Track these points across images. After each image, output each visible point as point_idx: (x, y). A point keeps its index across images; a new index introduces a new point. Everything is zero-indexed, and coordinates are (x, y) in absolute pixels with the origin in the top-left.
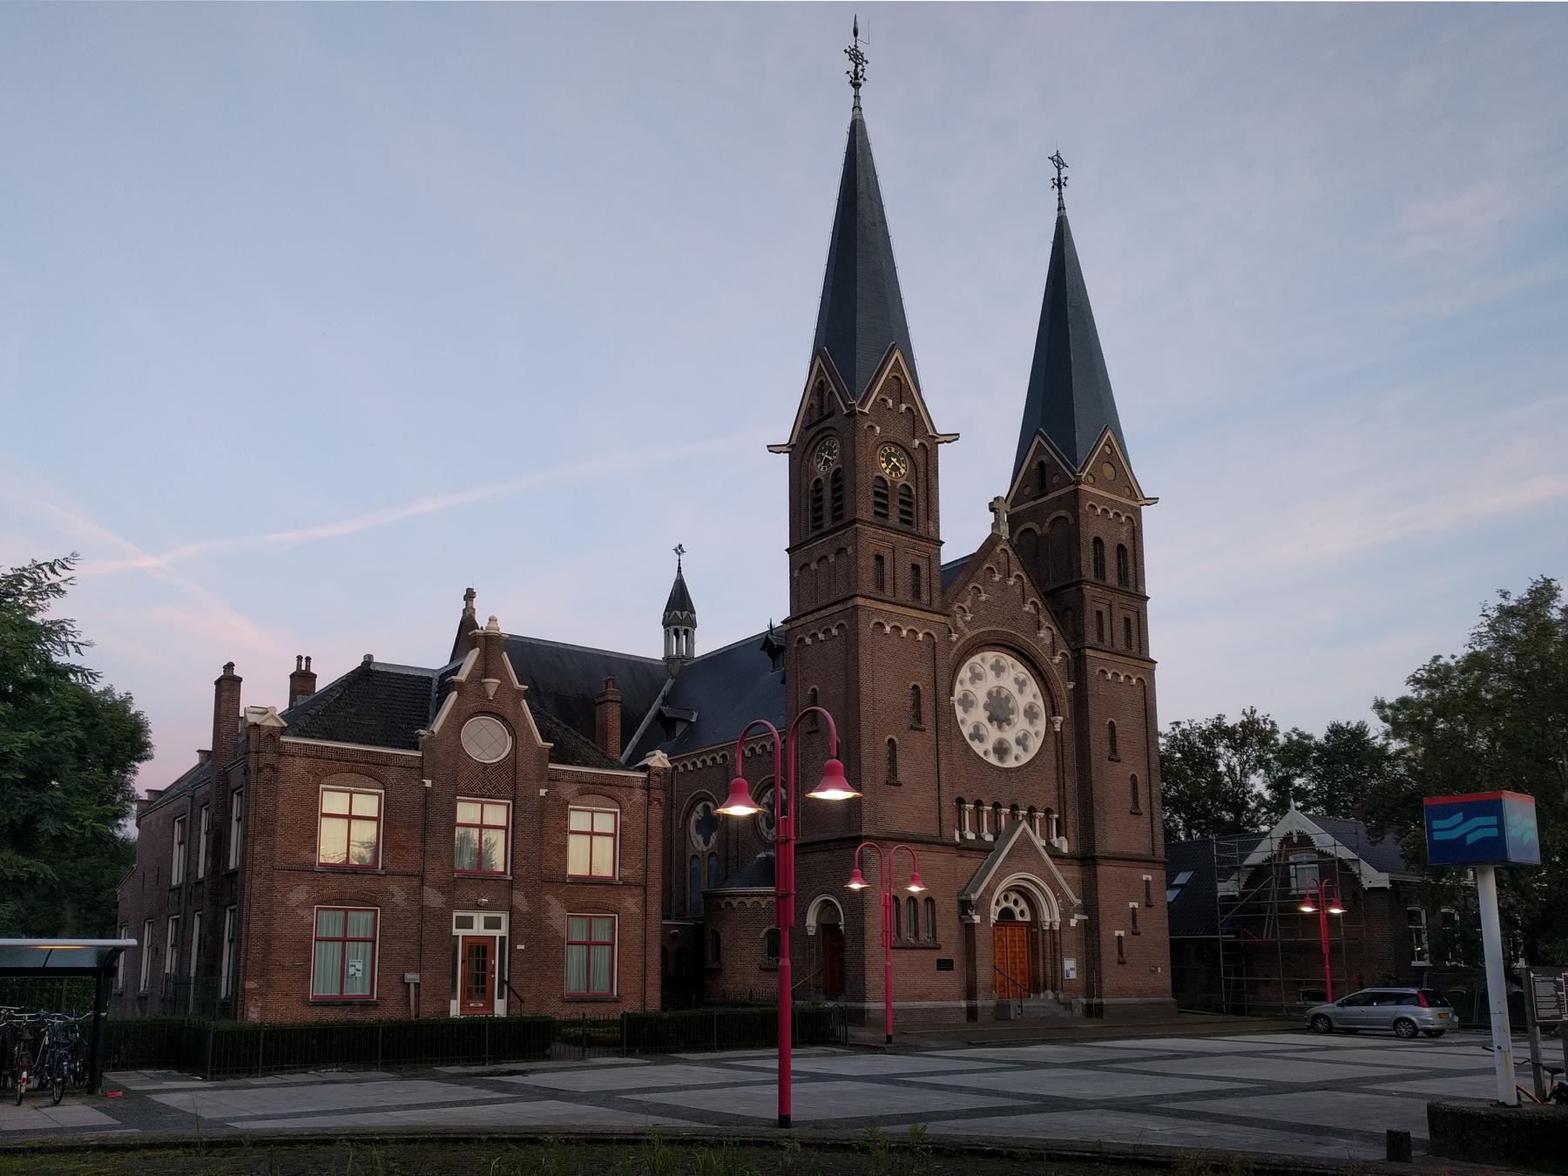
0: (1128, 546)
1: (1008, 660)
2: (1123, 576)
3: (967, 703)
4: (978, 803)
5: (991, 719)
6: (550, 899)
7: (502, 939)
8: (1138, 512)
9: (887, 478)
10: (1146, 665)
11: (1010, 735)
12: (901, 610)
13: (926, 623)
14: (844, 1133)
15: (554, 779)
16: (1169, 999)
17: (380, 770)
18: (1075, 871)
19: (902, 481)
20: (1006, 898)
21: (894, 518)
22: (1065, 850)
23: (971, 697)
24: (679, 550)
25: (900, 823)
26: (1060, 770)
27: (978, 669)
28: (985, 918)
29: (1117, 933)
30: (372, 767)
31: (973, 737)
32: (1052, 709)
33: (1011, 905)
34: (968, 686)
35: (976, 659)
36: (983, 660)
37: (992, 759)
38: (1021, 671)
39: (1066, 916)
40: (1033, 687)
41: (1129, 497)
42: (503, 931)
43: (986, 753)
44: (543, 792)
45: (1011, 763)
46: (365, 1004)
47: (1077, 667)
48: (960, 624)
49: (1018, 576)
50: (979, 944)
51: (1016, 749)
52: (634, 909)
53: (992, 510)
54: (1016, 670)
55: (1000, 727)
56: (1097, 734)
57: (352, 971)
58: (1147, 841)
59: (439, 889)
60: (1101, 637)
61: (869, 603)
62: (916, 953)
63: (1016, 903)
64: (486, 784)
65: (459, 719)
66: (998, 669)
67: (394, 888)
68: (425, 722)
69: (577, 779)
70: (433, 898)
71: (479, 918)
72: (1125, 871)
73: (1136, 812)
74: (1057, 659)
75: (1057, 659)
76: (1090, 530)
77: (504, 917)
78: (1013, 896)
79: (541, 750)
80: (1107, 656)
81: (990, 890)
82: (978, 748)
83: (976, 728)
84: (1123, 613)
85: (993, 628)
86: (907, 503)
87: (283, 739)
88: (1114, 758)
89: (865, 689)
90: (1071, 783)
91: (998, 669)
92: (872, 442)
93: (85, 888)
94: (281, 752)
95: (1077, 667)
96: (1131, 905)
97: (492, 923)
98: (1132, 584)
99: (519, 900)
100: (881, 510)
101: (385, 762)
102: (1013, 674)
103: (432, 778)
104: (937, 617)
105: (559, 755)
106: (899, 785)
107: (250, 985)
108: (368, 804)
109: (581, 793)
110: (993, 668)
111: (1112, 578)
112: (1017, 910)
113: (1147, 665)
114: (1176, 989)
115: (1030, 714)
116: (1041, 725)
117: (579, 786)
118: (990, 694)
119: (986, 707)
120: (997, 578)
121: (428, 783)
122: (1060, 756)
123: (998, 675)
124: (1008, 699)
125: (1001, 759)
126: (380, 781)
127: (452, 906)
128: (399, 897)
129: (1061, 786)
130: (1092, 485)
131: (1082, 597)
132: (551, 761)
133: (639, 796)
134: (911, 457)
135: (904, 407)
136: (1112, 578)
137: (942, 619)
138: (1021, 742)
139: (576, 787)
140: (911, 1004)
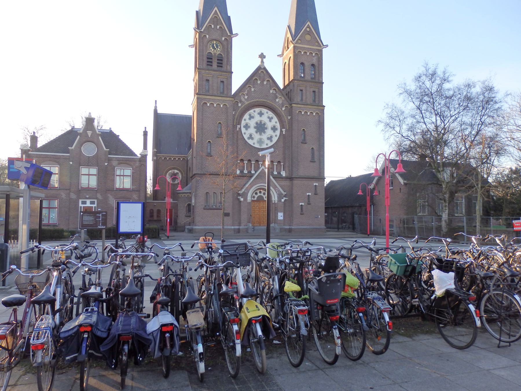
0: (316, 64)
1: (264, 110)
3: (247, 127)
4: (249, 161)
6: (109, 195)
8: (321, 51)
9: (212, 53)
10: (320, 108)
11: (264, 137)
12: (219, 98)
13: (224, 101)
19: (219, 53)
23: (249, 125)
25: (212, 169)
27: (252, 115)
28: (246, 199)
34: (248, 121)
35: (251, 111)
36: (254, 111)
38: (271, 114)
39: (280, 196)
40: (275, 119)
41: (317, 46)
42: (95, 205)
43: (254, 144)
44: (106, 164)
46: (54, 225)
47: (290, 111)
48: (243, 100)
49: (268, 80)
50: (242, 207)
54: (267, 113)
57: (51, 216)
62: (215, 211)
64: (89, 162)
65: (81, 144)
66: (261, 114)
67: (62, 193)
70: (73, 196)
71: (88, 201)
72: (305, 182)
73: (313, 161)
75: (284, 109)
77: (96, 201)
78: (258, 192)
79: (106, 151)
80: (302, 106)
81: (248, 189)
83: (251, 135)
84: (312, 90)
85: (258, 100)
87: (30, 153)
88: (304, 142)
91: (261, 114)
95: (290, 111)
97: (92, 203)
99: (99, 196)
101: (58, 158)
103: (72, 161)
109: (119, 164)
110: (258, 114)
113: (322, 108)
114: (327, 222)
115: (274, 129)
116: (278, 133)
118: (257, 123)
119: (261, 134)
120: (259, 82)
121: (71, 163)
123: (261, 116)
126: (130, 165)
127: (79, 198)
130: (300, 44)
132: (110, 155)
134: (222, 44)
135: (218, 27)
138: (270, 119)
139: (117, 162)
140: (212, 227)
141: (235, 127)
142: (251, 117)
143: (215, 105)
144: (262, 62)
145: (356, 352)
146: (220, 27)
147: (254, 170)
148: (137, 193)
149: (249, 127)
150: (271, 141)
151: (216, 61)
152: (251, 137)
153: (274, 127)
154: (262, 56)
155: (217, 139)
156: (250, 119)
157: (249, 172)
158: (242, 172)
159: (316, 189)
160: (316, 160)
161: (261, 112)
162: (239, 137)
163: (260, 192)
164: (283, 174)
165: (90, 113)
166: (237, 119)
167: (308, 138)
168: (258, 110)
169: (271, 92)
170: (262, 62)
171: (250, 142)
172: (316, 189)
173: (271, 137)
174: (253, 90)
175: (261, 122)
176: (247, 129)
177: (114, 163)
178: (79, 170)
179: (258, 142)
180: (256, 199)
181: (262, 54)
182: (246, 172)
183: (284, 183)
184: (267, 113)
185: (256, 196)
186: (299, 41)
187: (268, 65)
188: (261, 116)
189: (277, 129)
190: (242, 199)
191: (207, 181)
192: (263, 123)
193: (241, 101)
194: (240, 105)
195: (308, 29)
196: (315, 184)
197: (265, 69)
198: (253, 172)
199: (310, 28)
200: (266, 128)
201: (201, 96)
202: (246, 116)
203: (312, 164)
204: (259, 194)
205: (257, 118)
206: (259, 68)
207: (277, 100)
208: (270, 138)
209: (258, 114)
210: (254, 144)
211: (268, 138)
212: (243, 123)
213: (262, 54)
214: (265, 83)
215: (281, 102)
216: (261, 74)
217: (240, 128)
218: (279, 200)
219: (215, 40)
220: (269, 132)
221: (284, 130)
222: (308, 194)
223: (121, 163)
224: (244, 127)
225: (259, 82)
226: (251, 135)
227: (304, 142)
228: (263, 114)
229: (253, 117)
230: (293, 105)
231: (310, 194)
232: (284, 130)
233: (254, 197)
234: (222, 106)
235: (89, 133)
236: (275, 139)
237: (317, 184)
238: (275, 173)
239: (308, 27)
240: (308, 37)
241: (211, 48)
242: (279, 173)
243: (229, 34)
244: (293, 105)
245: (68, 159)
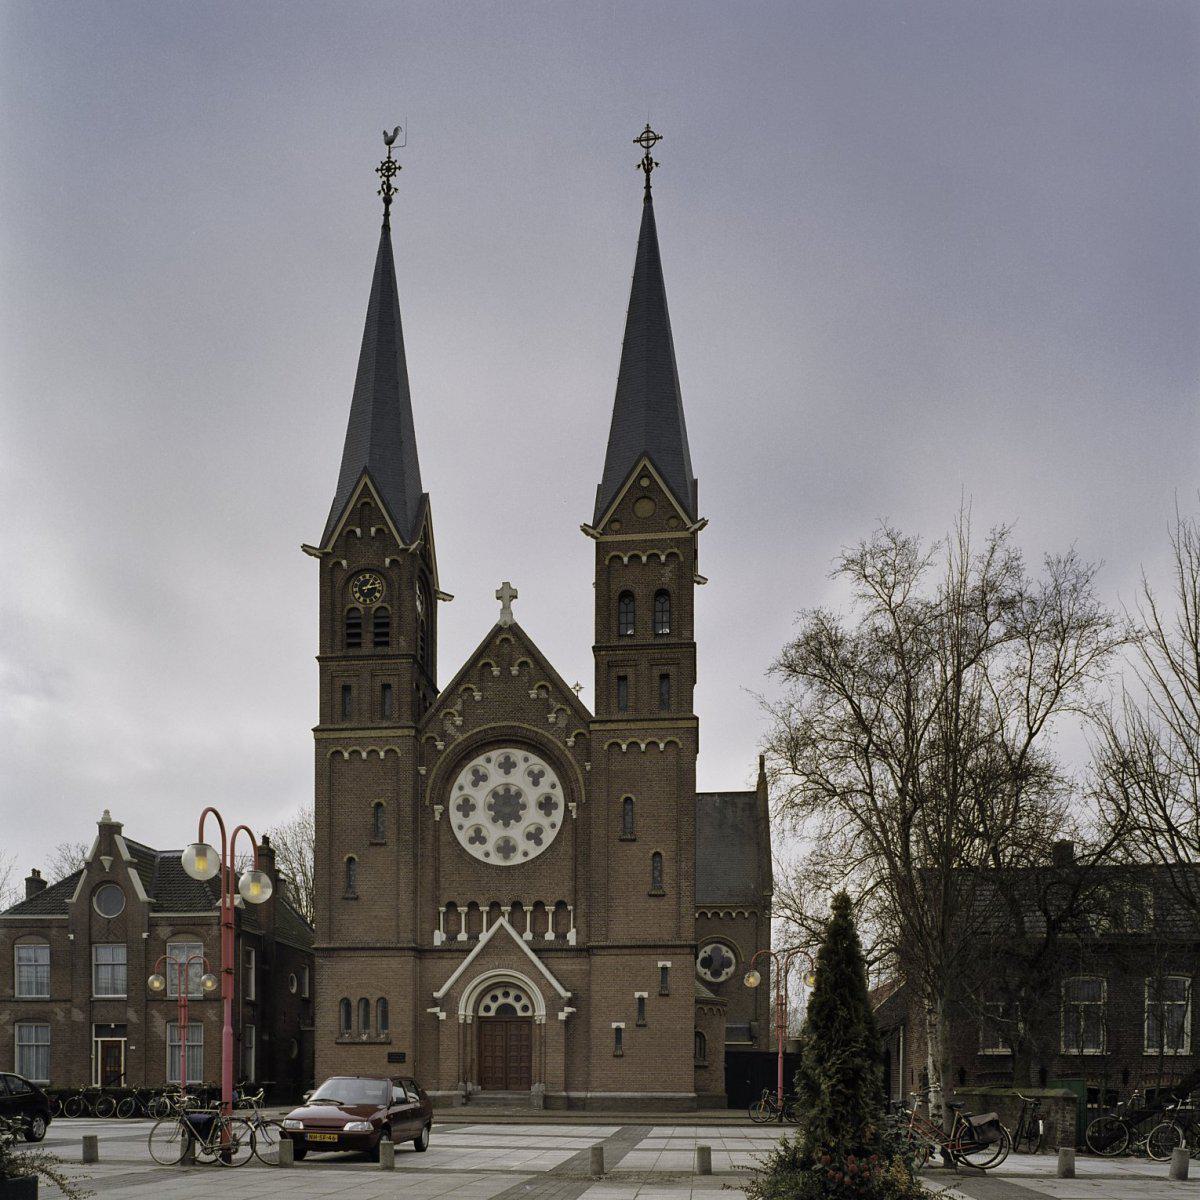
1: (517, 755)
3: (467, 807)
5: (518, 819)
8: (692, 542)
9: (361, 607)
13: (387, 740)
14: (206, 1169)
16: (725, 1094)
17: (202, 930)
19: (378, 604)
21: (368, 638)
23: (472, 801)
27: (482, 771)
28: (452, 1012)
30: (42, 930)
31: (472, 841)
32: (569, 796)
33: (510, 1000)
35: (479, 761)
37: (496, 860)
40: (551, 776)
44: (145, 935)
45: (517, 859)
48: (451, 730)
52: (214, 1018)
53: (498, 598)
54: (489, 762)
59: (80, 1009)
67: (57, 1010)
69: (171, 922)
75: (571, 742)
83: (478, 831)
85: (493, 725)
86: (353, 637)
91: (507, 766)
93: (1186, 1121)
101: (48, 925)
108: (44, 956)
109: (174, 934)
110: (500, 766)
115: (546, 805)
116: (558, 816)
117: (171, 928)
120: (496, 671)
123: (507, 772)
124: (519, 794)
125: (506, 857)
128: (60, 1016)
130: (617, 532)
138: (536, 777)
143: (364, 755)
144: (506, 609)
146: (378, 531)
147: (468, 931)
148: (149, 998)
149: (473, 807)
150: (539, 842)
151: (372, 629)
152: (478, 837)
153: (548, 798)
154: (507, 594)
155: (373, 849)
156: (475, 784)
159: (664, 980)
160: (667, 889)
161: (507, 758)
162: (444, 838)
165: (107, 812)
166: (432, 789)
168: (496, 755)
169: (533, 694)
170: (506, 609)
171: (476, 851)
172: (664, 980)
173: (539, 830)
174: (477, 696)
175: (507, 790)
176: (548, 798)
179: (499, 849)
180: (492, 1013)
181: (506, 585)
183: (568, 965)
184: (526, 760)
185: (494, 1006)
187: (525, 617)
188: (507, 772)
189: (555, 806)
190: (443, 1016)
191: (345, 966)
192: (513, 790)
193: (444, 736)
196: (660, 964)
197: (515, 629)
199: (650, 476)
201: (325, 735)
202: (465, 777)
203: (652, 902)
204: (501, 1000)
205: (517, 832)
206: (498, 630)
207: (552, 718)
208: (535, 836)
209: (514, 849)
210: (487, 855)
211: (529, 836)
212: (455, 797)
213: (506, 585)
214: (515, 671)
215: (562, 723)
216: (508, 647)
217: (445, 814)
220: (532, 816)
222: (637, 995)
224: (459, 808)
225: (496, 671)
226: (478, 831)
228: (514, 765)
229: (484, 778)
231: (645, 995)
233: (487, 1009)
234: (382, 754)
235: (106, 860)
236: (549, 837)
237: (669, 964)
239: (645, 474)
241: (357, 595)
245: (64, 927)
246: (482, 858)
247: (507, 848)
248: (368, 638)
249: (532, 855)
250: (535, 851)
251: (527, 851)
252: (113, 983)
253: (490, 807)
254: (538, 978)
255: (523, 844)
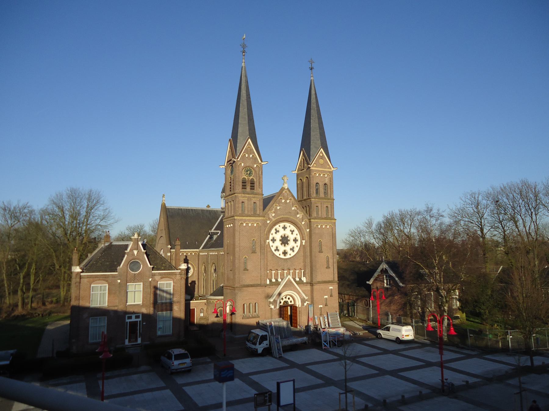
1: (287, 224)
2: (326, 193)
3: (274, 240)
7: (140, 321)
10: (333, 221)
11: (288, 248)
13: (257, 221)
15: (153, 275)
18: (308, 288)
20: (286, 297)
21: (248, 188)
22: (305, 281)
24: (311, 69)
25: (248, 282)
26: (305, 257)
29: (320, 306)
31: (275, 250)
32: (302, 238)
35: (277, 226)
37: (282, 256)
38: (293, 227)
39: (303, 301)
40: (296, 232)
42: (140, 319)
44: (150, 280)
45: (288, 256)
48: (271, 217)
51: (289, 252)
55: (285, 246)
56: (315, 245)
58: (332, 276)
60: (318, 213)
61: (238, 218)
63: (289, 299)
66: (284, 228)
68: (126, 250)
72: (322, 286)
73: (328, 267)
74: (303, 223)
75: (303, 223)
76: (313, 182)
80: (319, 220)
82: (277, 253)
83: (277, 247)
85: (282, 216)
88: (321, 251)
89: (237, 244)
90: (308, 260)
91: (284, 228)
92: (241, 169)
94: (81, 277)
96: (325, 297)
98: (329, 195)
100: (244, 187)
102: (274, 235)
104: (261, 218)
105: (153, 269)
106: (248, 270)
107: (74, 340)
109: (161, 278)
111: (322, 195)
112: (289, 301)
115: (295, 240)
116: (299, 243)
118: (281, 236)
122: (305, 252)
125: (285, 255)
129: (304, 262)
130: (315, 167)
131: (311, 203)
133: (178, 277)
135: (251, 156)
136: (322, 195)
137: (262, 218)
138: (292, 249)
139: (160, 277)
141: (265, 242)
142: (277, 231)
145: (457, 305)
149: (294, 240)
155: (252, 254)
157: (277, 280)
158: (271, 281)
160: (330, 266)
162: (268, 250)
163: (289, 299)
164: (304, 279)
167: (324, 248)
168: (282, 225)
169: (293, 209)
177: (157, 278)
178: (126, 287)
182: (274, 280)
185: (282, 302)
186: (315, 165)
189: (297, 240)
193: (269, 219)
194: (268, 222)
195: (321, 155)
198: (280, 280)
199: (322, 153)
200: (289, 240)
209: (287, 253)
212: (271, 237)
218: (303, 304)
219: (310, 231)
221: (304, 241)
223: (164, 278)
227: (321, 251)
230: (312, 220)
232: (304, 241)
236: (296, 250)
238: (297, 279)
240: (321, 161)
242: (300, 279)
243: (260, 162)
244: (312, 220)
246: (278, 255)
247: (285, 253)
248: (248, 188)
249: (292, 255)
250: (293, 254)
251: (290, 254)
252: (517, 393)
253: (280, 240)
254: (299, 293)
255: (281, 229)
